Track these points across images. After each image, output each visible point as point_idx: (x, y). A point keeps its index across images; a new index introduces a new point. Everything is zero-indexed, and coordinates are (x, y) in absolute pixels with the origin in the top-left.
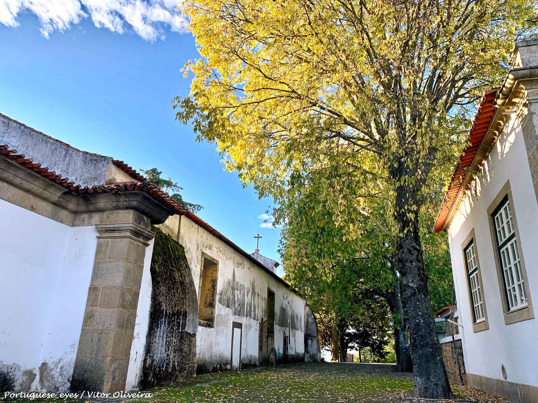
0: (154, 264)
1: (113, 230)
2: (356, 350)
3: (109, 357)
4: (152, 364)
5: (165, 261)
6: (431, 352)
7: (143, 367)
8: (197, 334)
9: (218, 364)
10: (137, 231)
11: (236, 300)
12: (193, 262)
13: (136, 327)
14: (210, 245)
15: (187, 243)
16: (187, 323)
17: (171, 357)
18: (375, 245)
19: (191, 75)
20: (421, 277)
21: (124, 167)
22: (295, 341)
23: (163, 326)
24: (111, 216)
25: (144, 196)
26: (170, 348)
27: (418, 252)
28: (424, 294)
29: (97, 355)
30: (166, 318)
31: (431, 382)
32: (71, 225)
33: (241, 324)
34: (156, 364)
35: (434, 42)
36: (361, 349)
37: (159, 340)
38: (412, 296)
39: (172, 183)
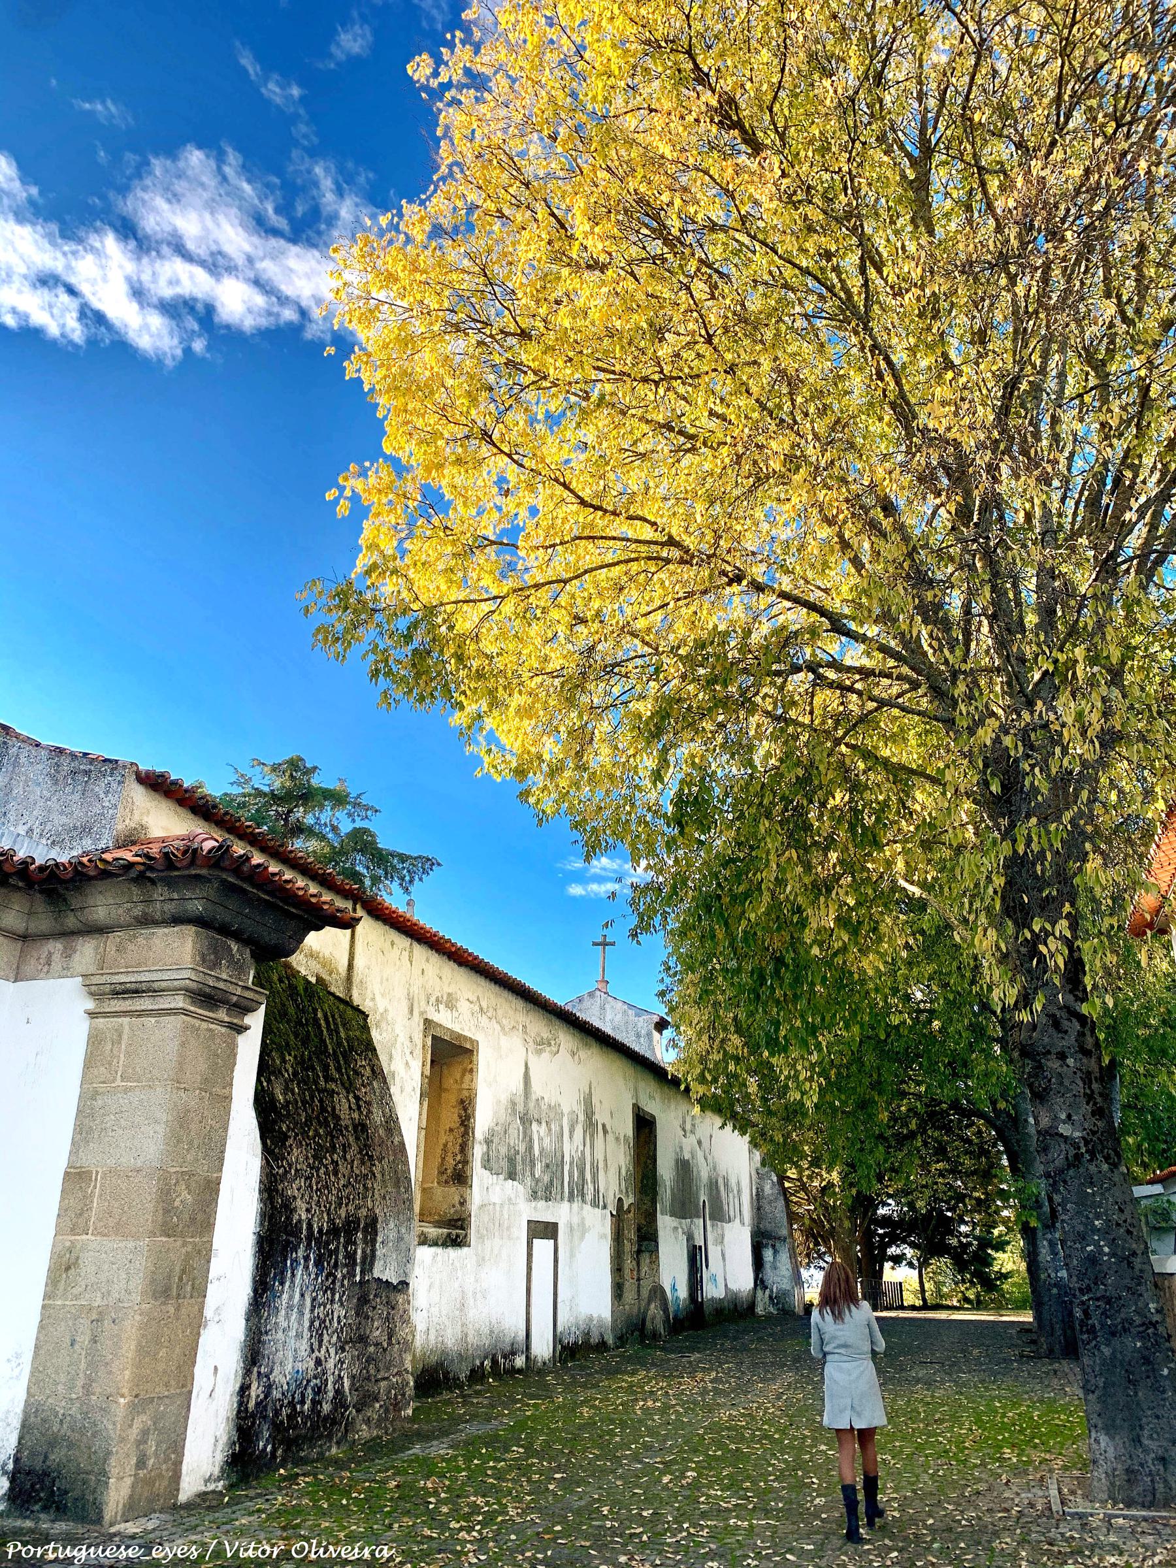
0: (269, 1081)
1: (135, 992)
2: (911, 1265)
3: (123, 1396)
4: (266, 1397)
5: (304, 1064)
6: (1139, 1350)
7: (239, 1412)
8: (413, 1284)
9: (486, 1358)
10: (208, 990)
11: (537, 1153)
12: (397, 1054)
13: (211, 1289)
14: (449, 995)
15: (378, 997)
16: (378, 1253)
17: (331, 1364)
18: (949, 974)
19: (360, 510)
20: (1095, 1104)
21: (173, 788)
22: (723, 1255)
23: (299, 1272)
24: (131, 947)
25: (224, 882)
26: (326, 1338)
27: (1083, 1025)
28: (1107, 1158)
29: (87, 1389)
30: (308, 1247)
31: (1146, 1451)
32: (12, 975)
33: (555, 1225)
34: (279, 1396)
35: (1099, 367)
36: (923, 1264)
37: (287, 1317)
38: (1069, 1168)
39: (347, 795)
